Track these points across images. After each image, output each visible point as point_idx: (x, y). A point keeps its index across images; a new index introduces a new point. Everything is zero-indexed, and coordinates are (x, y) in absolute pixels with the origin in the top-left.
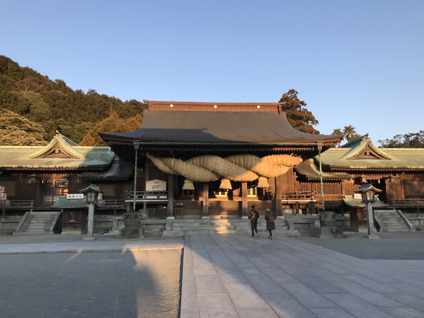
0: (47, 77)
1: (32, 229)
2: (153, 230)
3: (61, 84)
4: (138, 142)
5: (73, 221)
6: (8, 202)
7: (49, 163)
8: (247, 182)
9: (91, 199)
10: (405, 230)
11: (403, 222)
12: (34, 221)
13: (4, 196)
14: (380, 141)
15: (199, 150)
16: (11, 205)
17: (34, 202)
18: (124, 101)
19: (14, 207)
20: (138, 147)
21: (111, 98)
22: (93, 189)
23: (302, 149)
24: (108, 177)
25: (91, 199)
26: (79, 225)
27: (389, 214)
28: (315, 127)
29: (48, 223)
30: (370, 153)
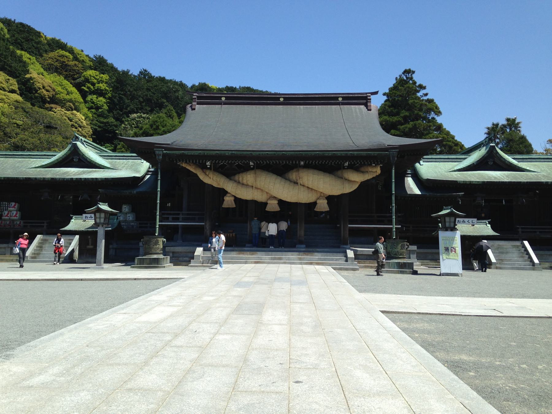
13: (16, 214)
28: (439, 120)
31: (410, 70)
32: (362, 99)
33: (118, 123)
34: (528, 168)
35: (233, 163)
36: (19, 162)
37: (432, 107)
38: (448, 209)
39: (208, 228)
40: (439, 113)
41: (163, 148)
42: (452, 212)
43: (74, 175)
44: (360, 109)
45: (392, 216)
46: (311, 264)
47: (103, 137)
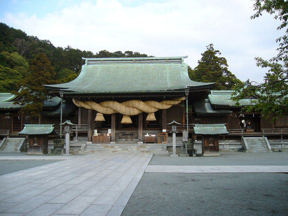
1: (7, 149)
2: (74, 150)
4: (63, 92)
5: (36, 144)
10: (265, 151)
11: (266, 145)
12: (9, 144)
15: (104, 97)
17: (9, 131)
22: (68, 124)
23: (67, 93)
24: (55, 115)
26: (41, 148)
27: (258, 140)
29: (17, 145)
35: (101, 98)
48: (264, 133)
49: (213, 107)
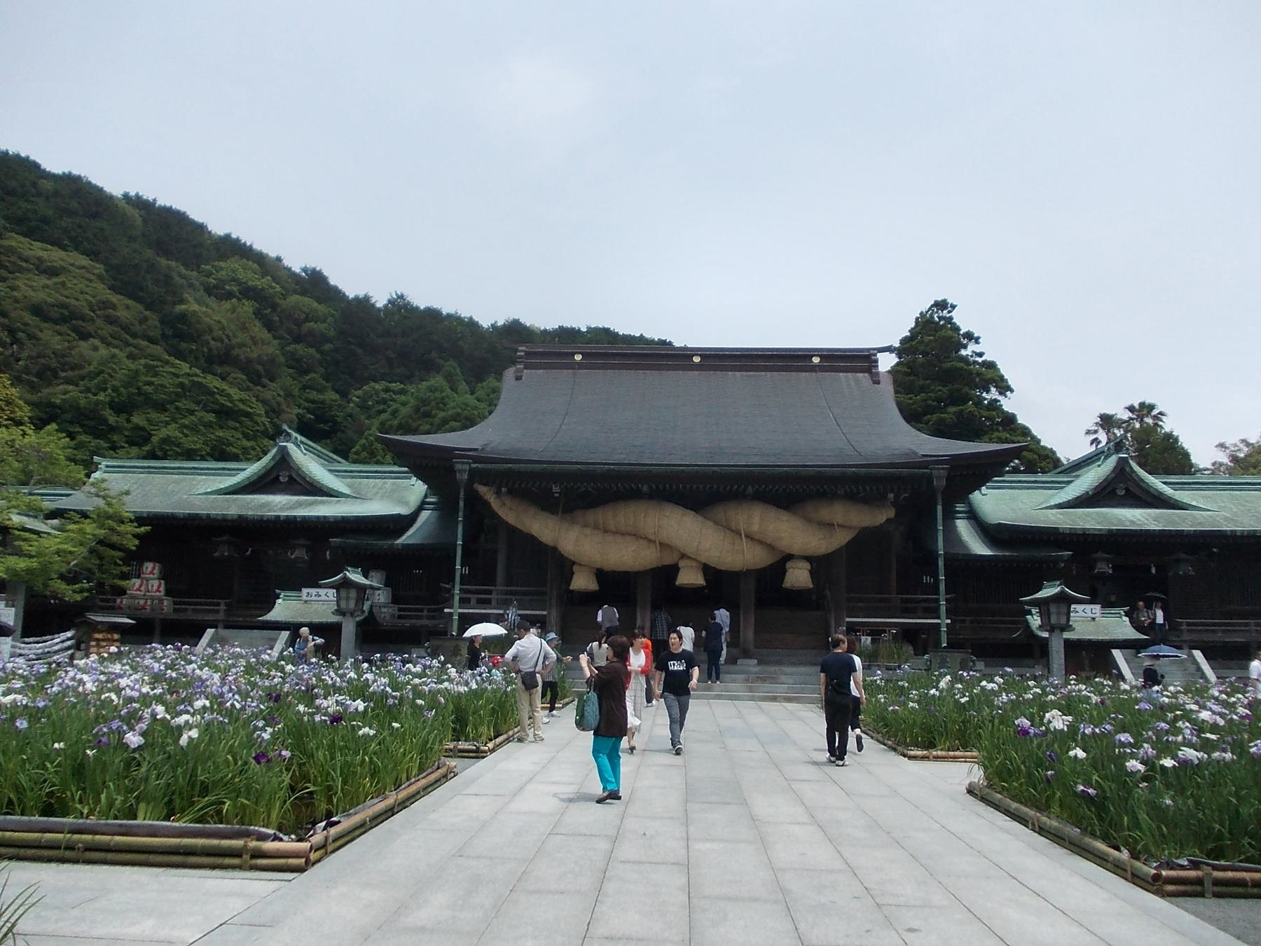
0: (279, 259)
3: (315, 283)
6: (167, 603)
7: (263, 505)
8: (808, 558)
9: (347, 604)
13: (159, 586)
14: (1222, 446)
16: (175, 610)
17: (226, 605)
18: (485, 323)
19: (182, 616)
20: (466, 476)
21: (449, 316)
25: (347, 604)
28: (1008, 404)
30: (1127, 489)
31: (944, 301)
32: (862, 361)
33: (343, 403)
34: (1194, 503)
35: (587, 489)
36: (175, 482)
37: (991, 376)
38: (1053, 586)
39: (553, 622)
40: (1004, 388)
41: (468, 457)
42: (1062, 592)
43: (281, 509)
44: (857, 381)
45: (937, 601)
46: (774, 699)
47: (326, 432)
48: (1186, 637)
49: (991, 532)
